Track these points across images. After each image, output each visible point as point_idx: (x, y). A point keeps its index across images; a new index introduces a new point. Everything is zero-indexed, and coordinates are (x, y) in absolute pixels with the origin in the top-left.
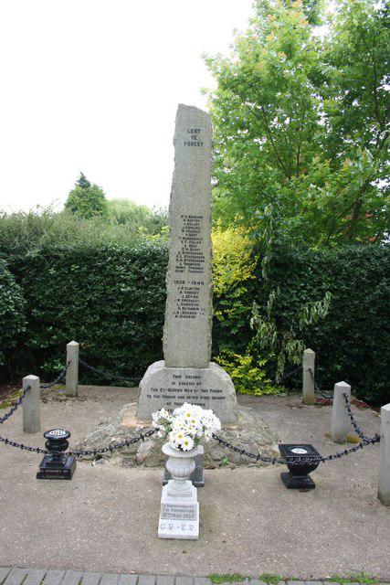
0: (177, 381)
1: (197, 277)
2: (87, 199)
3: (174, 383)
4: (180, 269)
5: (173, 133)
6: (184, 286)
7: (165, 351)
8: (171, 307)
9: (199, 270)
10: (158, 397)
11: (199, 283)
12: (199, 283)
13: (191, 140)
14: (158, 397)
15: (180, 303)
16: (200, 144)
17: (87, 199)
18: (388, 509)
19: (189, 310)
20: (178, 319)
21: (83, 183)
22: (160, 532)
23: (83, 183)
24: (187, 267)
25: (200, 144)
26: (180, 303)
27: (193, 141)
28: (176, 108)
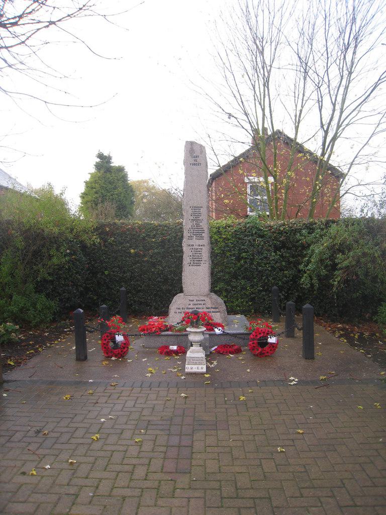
0: (191, 303)
1: (201, 242)
2: (108, 182)
3: (190, 304)
4: (190, 238)
5: (183, 158)
6: (193, 247)
7: (184, 289)
8: (186, 260)
9: (202, 238)
10: (181, 313)
11: (202, 246)
12: (202, 246)
13: (193, 162)
14: (181, 313)
15: (191, 258)
16: (199, 164)
17: (108, 182)
18: (100, 512)
19: (197, 262)
20: (191, 267)
21: (104, 162)
22: (186, 370)
23: (104, 162)
24: (195, 236)
25: (199, 164)
26: (191, 258)
27: (196, 163)
28: (184, 143)
